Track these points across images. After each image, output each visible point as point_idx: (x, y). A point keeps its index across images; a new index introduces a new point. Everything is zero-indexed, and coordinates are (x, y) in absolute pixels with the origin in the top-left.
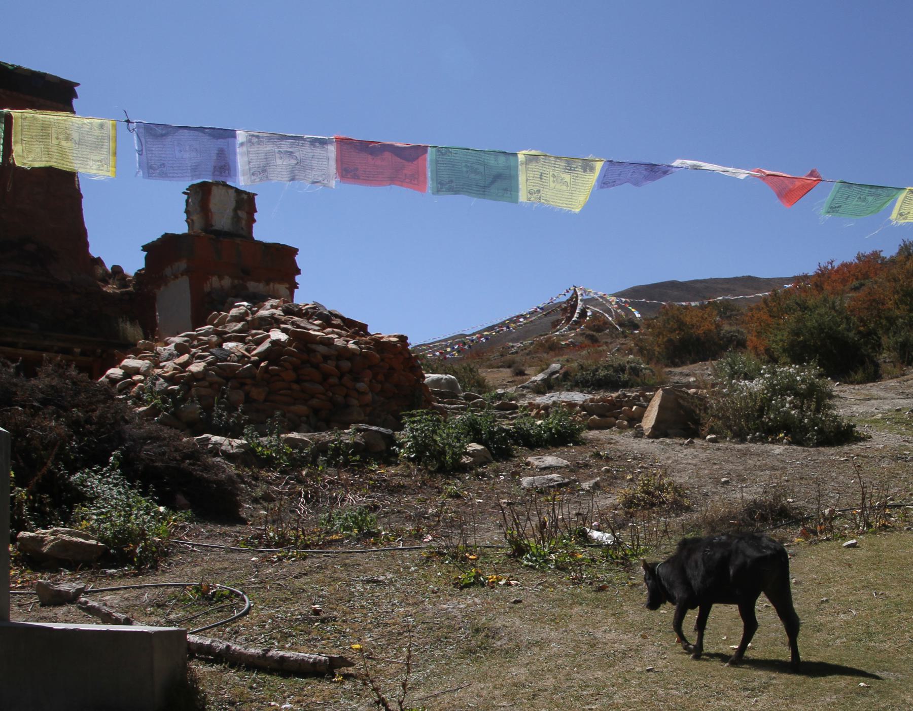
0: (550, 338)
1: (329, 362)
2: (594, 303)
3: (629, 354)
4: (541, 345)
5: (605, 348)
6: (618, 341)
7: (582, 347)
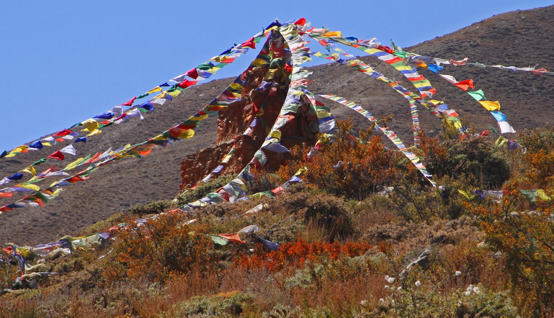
0: (172, 221)
1: (546, 210)
2: (344, 81)
3: (465, 281)
4: (135, 250)
5: (377, 257)
6: (425, 229)
7: (291, 253)
